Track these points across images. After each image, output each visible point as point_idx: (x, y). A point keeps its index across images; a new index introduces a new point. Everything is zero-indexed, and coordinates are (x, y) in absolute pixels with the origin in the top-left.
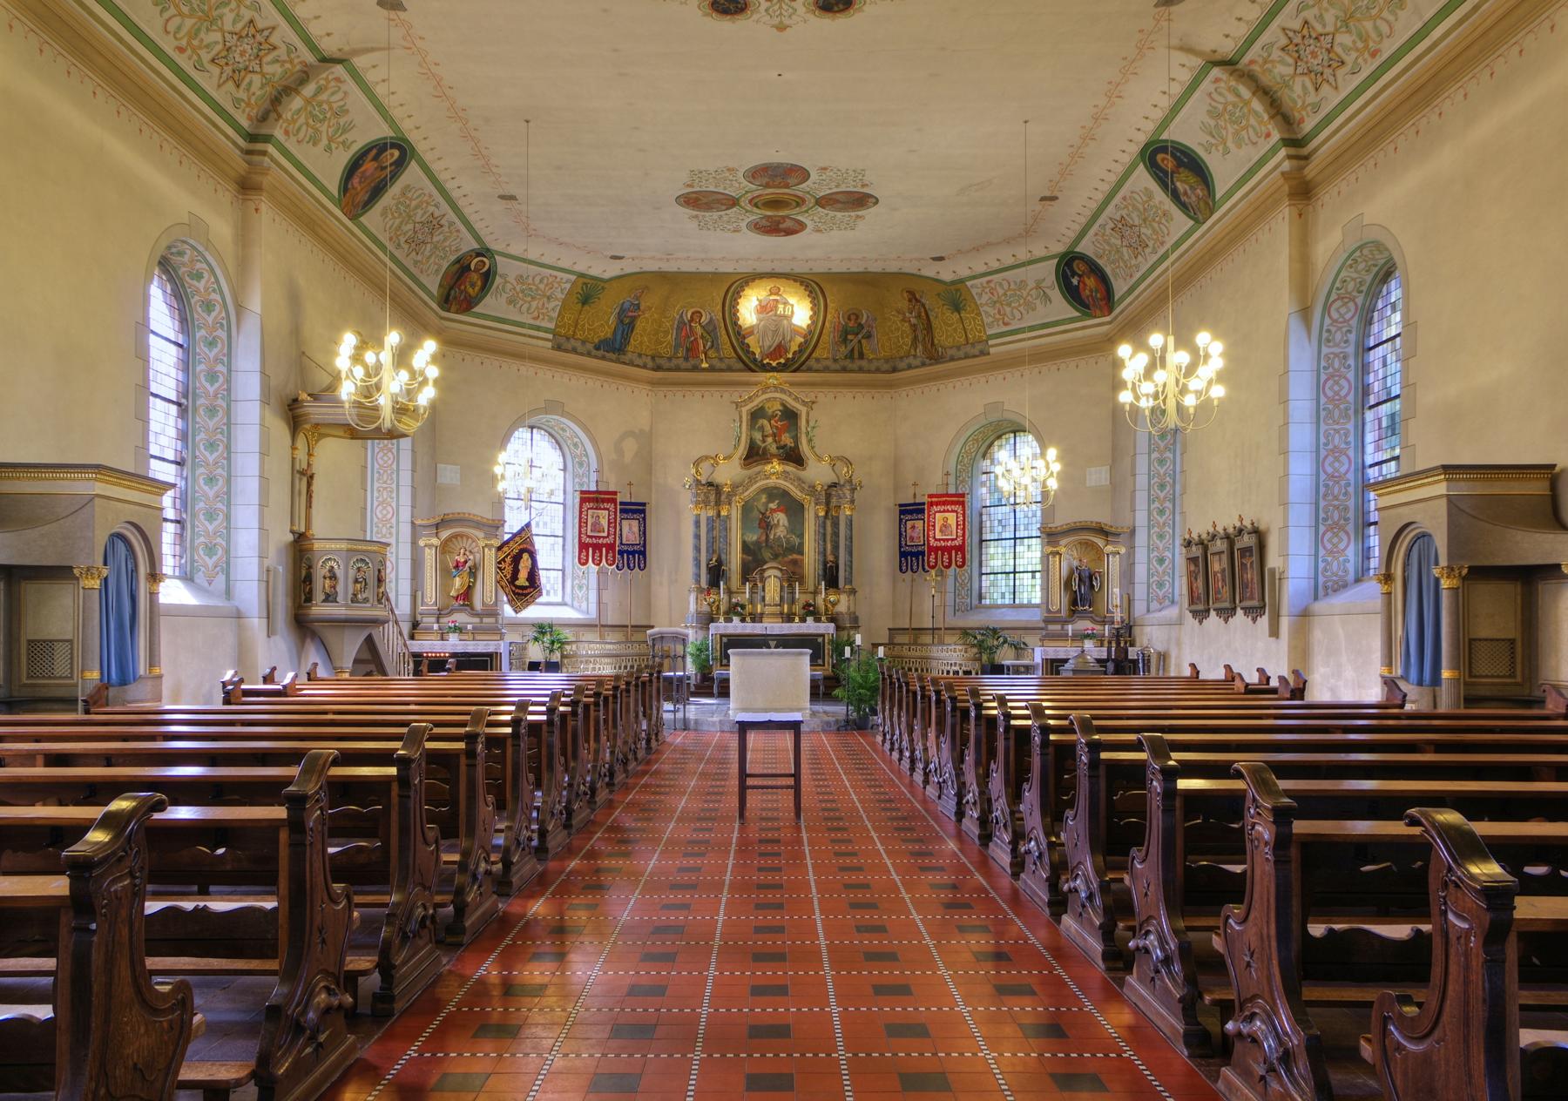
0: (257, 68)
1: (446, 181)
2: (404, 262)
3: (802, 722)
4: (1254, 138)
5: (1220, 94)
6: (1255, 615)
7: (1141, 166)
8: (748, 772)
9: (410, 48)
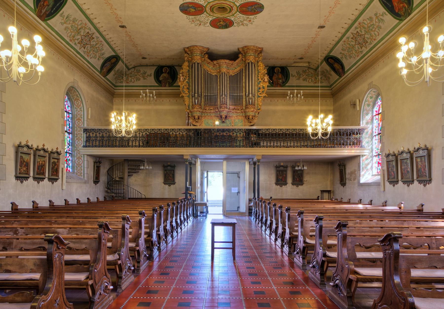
0: (82, 37)
1: (110, 42)
2: (79, 51)
3: (236, 223)
4: (354, 56)
5: (345, 45)
6: (394, 184)
7: (324, 62)
8: (215, 241)
9: (112, 13)
